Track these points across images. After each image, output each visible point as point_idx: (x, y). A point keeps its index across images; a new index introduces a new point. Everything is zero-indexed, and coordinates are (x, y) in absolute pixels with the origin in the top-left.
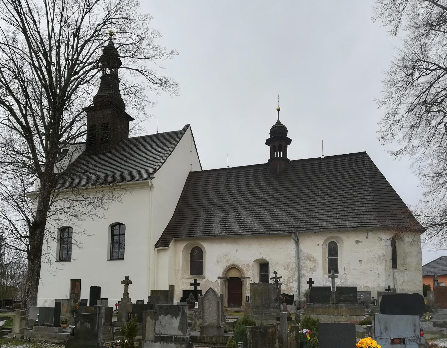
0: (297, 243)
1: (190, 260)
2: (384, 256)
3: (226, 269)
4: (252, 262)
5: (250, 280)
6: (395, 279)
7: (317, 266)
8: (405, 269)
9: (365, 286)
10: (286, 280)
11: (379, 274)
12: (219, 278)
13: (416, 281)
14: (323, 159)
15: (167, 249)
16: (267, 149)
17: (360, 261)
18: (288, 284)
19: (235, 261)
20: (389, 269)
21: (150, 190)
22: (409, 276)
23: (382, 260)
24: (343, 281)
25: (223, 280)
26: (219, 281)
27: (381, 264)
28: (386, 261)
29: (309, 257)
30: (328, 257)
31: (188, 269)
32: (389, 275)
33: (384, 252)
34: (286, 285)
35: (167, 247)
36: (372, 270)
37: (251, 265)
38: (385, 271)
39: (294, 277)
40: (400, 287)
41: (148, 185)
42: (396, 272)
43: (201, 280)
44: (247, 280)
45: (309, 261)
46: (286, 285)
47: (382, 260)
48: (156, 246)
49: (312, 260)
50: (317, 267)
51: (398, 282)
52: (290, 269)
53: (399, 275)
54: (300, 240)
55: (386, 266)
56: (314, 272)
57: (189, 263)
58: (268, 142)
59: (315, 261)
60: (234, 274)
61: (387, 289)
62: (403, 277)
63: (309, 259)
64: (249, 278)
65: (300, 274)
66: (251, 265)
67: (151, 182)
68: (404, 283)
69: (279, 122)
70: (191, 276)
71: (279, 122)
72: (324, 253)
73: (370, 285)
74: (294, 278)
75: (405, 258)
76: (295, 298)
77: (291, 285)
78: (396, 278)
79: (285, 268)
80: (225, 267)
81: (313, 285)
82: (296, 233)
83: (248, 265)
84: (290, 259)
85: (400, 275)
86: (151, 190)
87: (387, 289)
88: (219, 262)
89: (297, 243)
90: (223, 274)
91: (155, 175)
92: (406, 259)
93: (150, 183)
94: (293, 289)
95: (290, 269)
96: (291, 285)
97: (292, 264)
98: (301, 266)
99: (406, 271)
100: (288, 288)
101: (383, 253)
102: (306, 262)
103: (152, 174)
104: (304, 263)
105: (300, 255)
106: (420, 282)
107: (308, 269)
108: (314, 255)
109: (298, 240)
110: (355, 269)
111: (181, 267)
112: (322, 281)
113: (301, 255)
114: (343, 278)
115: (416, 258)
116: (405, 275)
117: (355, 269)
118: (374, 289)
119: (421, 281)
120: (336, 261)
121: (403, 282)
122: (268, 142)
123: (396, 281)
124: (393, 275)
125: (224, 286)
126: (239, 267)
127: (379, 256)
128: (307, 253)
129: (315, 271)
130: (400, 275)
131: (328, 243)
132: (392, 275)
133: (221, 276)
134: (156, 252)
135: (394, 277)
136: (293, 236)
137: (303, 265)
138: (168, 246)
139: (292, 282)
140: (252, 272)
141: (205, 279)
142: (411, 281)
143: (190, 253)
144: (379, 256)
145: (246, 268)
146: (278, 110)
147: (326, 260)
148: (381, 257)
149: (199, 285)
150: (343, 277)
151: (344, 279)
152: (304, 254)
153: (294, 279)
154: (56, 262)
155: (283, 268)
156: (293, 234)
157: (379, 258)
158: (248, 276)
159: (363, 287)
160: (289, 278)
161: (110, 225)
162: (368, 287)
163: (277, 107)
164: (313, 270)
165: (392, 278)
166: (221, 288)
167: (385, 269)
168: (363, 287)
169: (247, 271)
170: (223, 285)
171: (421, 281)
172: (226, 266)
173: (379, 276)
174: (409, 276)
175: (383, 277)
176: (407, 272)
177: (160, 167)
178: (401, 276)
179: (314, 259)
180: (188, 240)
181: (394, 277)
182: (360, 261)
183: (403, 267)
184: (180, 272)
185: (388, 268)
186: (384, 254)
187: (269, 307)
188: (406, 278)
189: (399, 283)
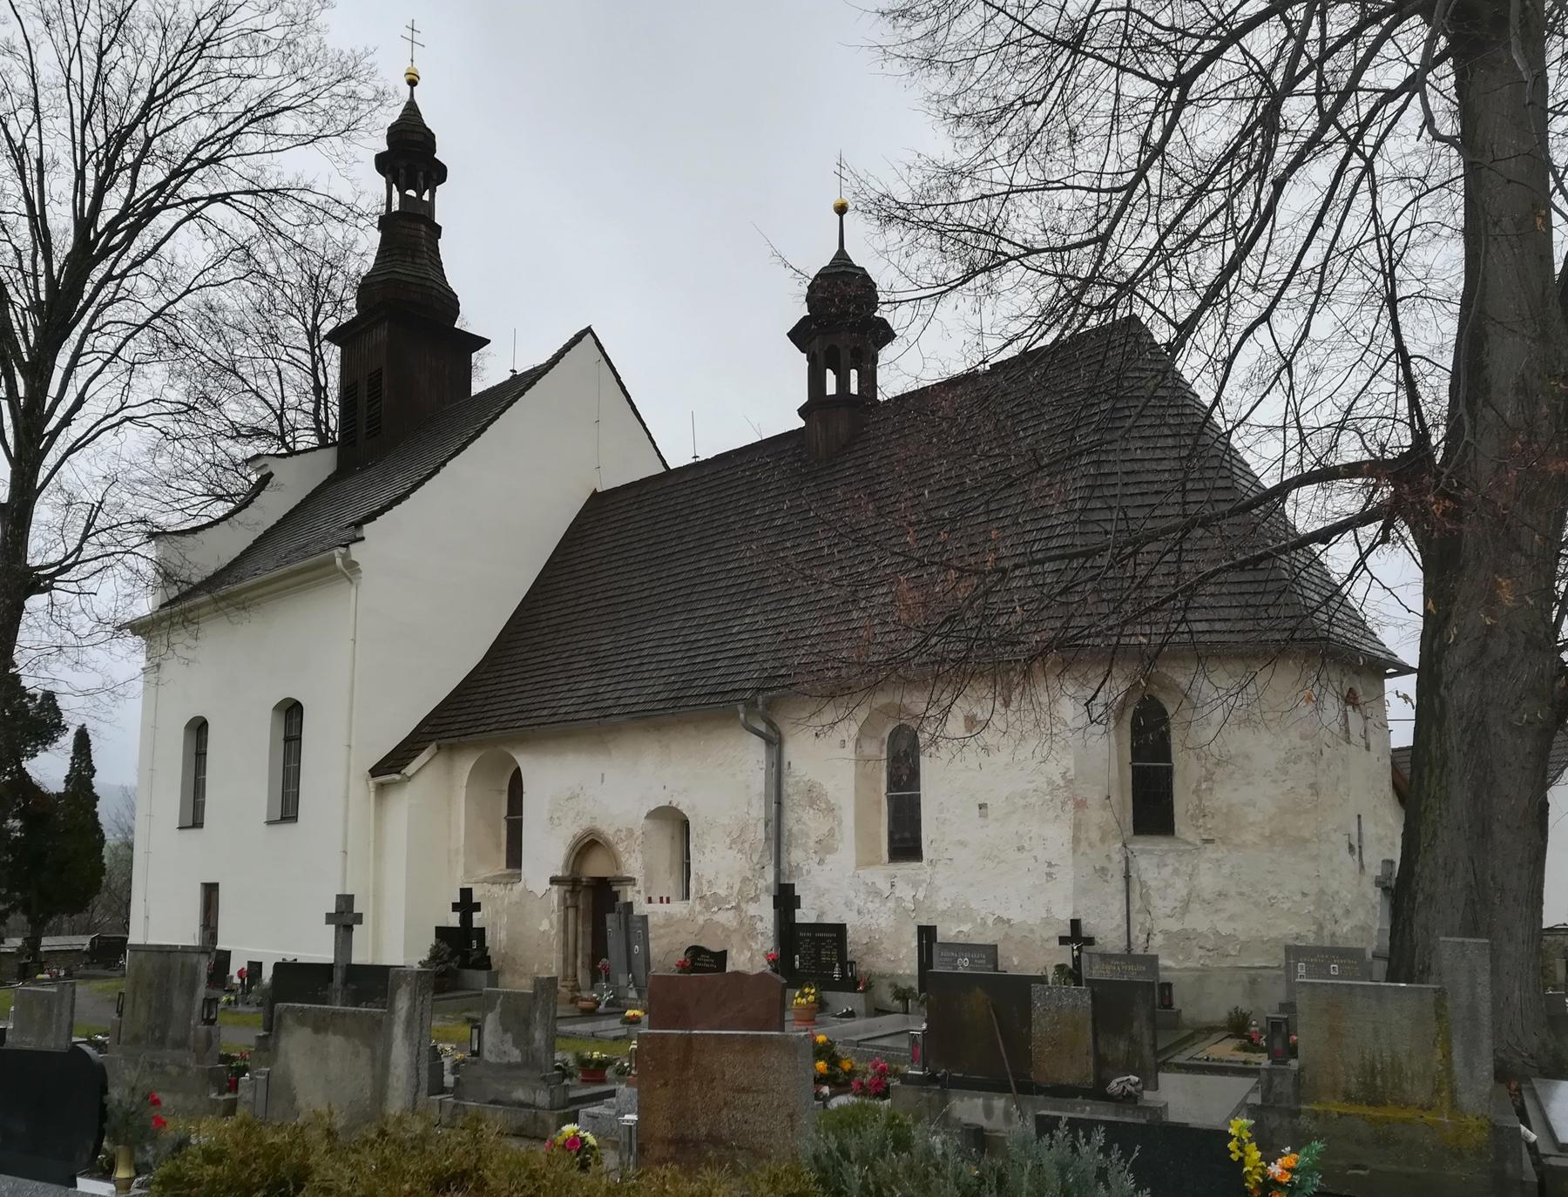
0: (774, 742)
1: (505, 812)
2: (1071, 781)
3: (573, 849)
4: (642, 821)
5: (636, 888)
6: (1136, 888)
7: (837, 829)
8: (1205, 837)
9: (999, 919)
10: (736, 889)
11: (1050, 865)
12: (554, 881)
13: (1273, 892)
14: (987, 374)
15: (395, 783)
16: (798, 362)
17: (981, 806)
18: (743, 905)
20: (1103, 840)
21: (348, 583)
22: (1226, 870)
23: (1064, 803)
24: (920, 896)
25: (565, 888)
26: (555, 893)
27: (1057, 816)
28: (1080, 805)
29: (813, 796)
30: (889, 790)
31: (498, 846)
32: (1103, 870)
33: (1071, 764)
34: (737, 908)
35: (397, 777)
36: (1023, 847)
37: (638, 833)
38: (1075, 851)
39: (762, 876)
40: (1174, 925)
41: (337, 570)
42: (1143, 852)
43: (509, 886)
44: (629, 888)
45: (811, 812)
46: (737, 908)
47: (1064, 803)
48: (375, 771)
49: (823, 805)
50: (837, 835)
51: (1156, 901)
52: (747, 845)
53: (1161, 865)
54: (786, 728)
55: (1077, 826)
56: (829, 858)
57: (504, 824)
58: (799, 335)
59: (831, 810)
60: (596, 867)
61: (1068, 933)
62: (1191, 876)
63: (812, 803)
64: (631, 881)
65: (784, 865)
66: (638, 833)
67: (345, 557)
68: (1194, 906)
69: (841, 254)
70: (509, 871)
71: (841, 254)
72: (861, 777)
73: (1015, 915)
74: (762, 881)
75: (1204, 786)
76: (28, 935)
77: (752, 909)
78: (1143, 884)
79: (733, 841)
80: (570, 840)
81: (804, 915)
82: (755, 704)
83: (630, 832)
84: (749, 804)
85: (1169, 869)
86: (351, 582)
87: (1068, 933)
88: (556, 822)
89: (774, 742)
90: (566, 866)
91: (368, 529)
92: (1210, 789)
93: (339, 561)
94: (759, 925)
95: (747, 845)
96: (752, 909)
97: (756, 825)
98: (790, 831)
99: (1208, 846)
100: (741, 923)
101: (1068, 769)
102: (805, 817)
103: (358, 525)
104: (798, 821)
105: (785, 786)
106: (1298, 898)
107: (811, 843)
108: (829, 786)
109: (771, 724)
110: (963, 844)
111: (462, 843)
112: (852, 894)
113: (788, 789)
114: (924, 881)
115: (1275, 781)
116: (1204, 866)
117: (963, 844)
118: (1032, 931)
119: (1304, 895)
120: (915, 804)
121: (1186, 903)
122: (799, 335)
123: (1145, 897)
124: (1123, 865)
125: (571, 912)
126: (607, 842)
127: (1050, 782)
128: (806, 779)
129: (831, 850)
130: (1169, 869)
131: (886, 735)
132: (1117, 868)
133: (559, 874)
134: (372, 795)
135: (1127, 877)
136: (742, 716)
137: (795, 829)
138: (399, 773)
139: (755, 899)
140: (640, 857)
141: (518, 887)
142: (1241, 894)
143: (506, 787)
144: (1050, 782)
146: (841, 210)
147: (879, 803)
148: (1059, 787)
149: (477, 907)
150: (921, 878)
151: (925, 885)
152: (798, 782)
153: (761, 883)
154: (180, 828)
155: (728, 841)
156: (740, 707)
157: (1051, 793)
159: (990, 922)
160: (745, 880)
161: (277, 708)
162: (1009, 920)
163: (835, 199)
164: (825, 846)
165: (1118, 882)
166: (559, 917)
167: (1076, 840)
168: (990, 922)
171: (1304, 895)
173: (1049, 875)
174: (1226, 870)
175: (1066, 878)
176: (1210, 852)
177: (405, 496)
178: (1176, 872)
179: (827, 802)
180: (477, 745)
181: (1127, 877)
182: (981, 806)
183: (1198, 827)
184: (462, 859)
185: (1095, 835)
186: (1071, 773)
187: (161, 1042)
188: (1207, 880)
189: (1161, 906)
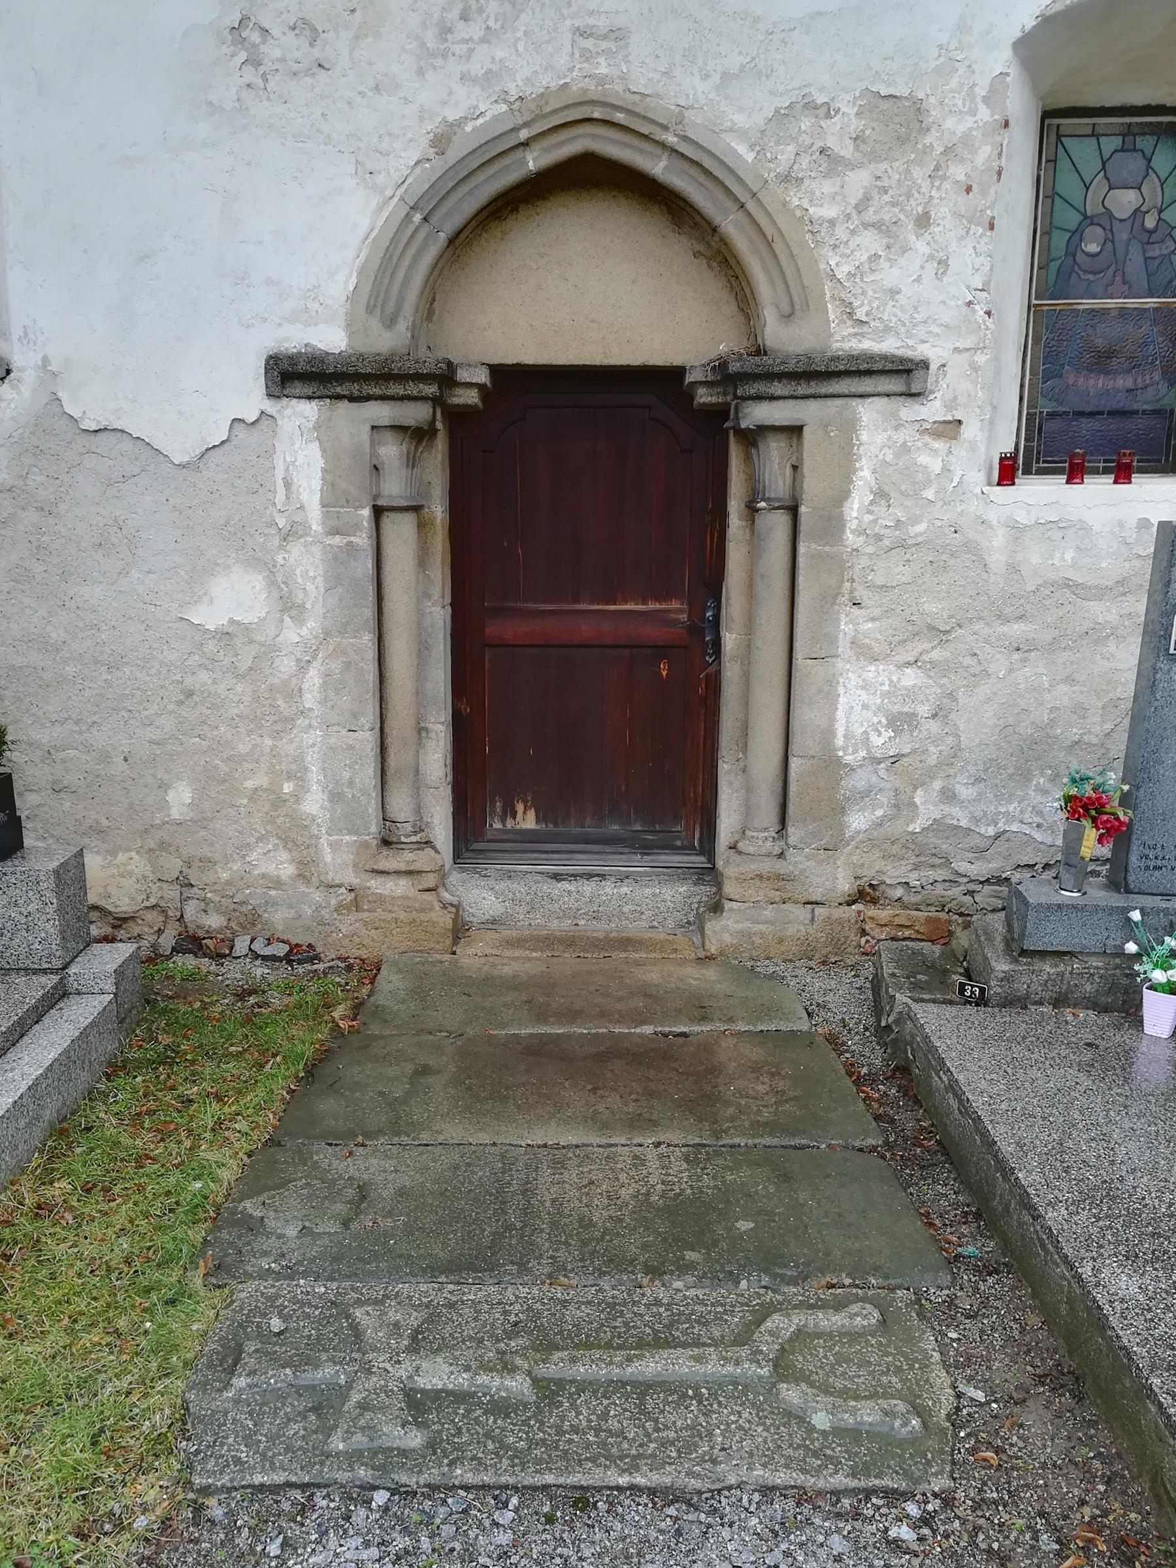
5: (932, 410)
19: (617, 35)
25: (382, 412)
44: (868, 413)
81: (714, 889)
125: (400, 530)
145: (858, 181)
158: (889, 346)
169: (871, 242)
170: (378, 512)
172: (440, 142)
